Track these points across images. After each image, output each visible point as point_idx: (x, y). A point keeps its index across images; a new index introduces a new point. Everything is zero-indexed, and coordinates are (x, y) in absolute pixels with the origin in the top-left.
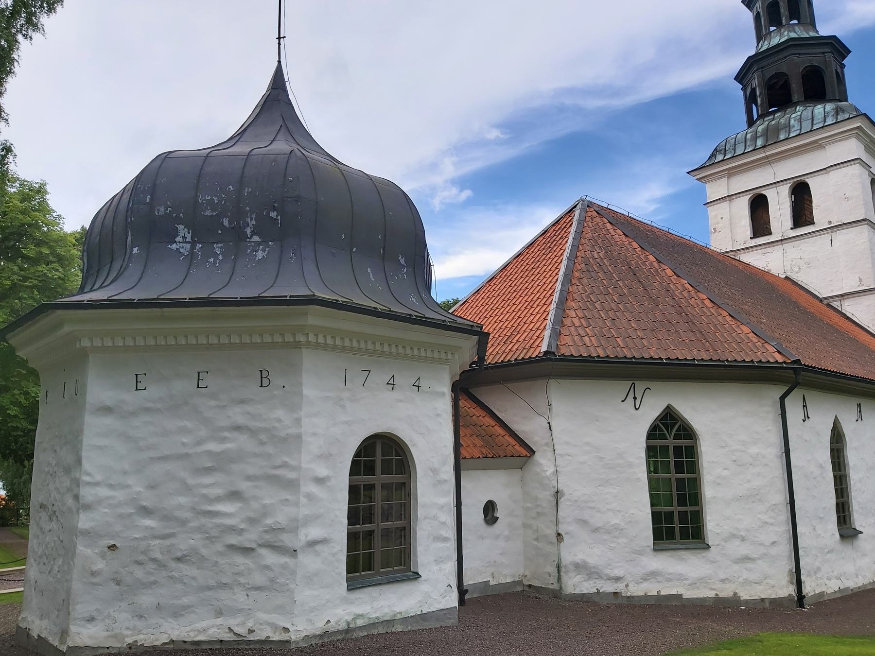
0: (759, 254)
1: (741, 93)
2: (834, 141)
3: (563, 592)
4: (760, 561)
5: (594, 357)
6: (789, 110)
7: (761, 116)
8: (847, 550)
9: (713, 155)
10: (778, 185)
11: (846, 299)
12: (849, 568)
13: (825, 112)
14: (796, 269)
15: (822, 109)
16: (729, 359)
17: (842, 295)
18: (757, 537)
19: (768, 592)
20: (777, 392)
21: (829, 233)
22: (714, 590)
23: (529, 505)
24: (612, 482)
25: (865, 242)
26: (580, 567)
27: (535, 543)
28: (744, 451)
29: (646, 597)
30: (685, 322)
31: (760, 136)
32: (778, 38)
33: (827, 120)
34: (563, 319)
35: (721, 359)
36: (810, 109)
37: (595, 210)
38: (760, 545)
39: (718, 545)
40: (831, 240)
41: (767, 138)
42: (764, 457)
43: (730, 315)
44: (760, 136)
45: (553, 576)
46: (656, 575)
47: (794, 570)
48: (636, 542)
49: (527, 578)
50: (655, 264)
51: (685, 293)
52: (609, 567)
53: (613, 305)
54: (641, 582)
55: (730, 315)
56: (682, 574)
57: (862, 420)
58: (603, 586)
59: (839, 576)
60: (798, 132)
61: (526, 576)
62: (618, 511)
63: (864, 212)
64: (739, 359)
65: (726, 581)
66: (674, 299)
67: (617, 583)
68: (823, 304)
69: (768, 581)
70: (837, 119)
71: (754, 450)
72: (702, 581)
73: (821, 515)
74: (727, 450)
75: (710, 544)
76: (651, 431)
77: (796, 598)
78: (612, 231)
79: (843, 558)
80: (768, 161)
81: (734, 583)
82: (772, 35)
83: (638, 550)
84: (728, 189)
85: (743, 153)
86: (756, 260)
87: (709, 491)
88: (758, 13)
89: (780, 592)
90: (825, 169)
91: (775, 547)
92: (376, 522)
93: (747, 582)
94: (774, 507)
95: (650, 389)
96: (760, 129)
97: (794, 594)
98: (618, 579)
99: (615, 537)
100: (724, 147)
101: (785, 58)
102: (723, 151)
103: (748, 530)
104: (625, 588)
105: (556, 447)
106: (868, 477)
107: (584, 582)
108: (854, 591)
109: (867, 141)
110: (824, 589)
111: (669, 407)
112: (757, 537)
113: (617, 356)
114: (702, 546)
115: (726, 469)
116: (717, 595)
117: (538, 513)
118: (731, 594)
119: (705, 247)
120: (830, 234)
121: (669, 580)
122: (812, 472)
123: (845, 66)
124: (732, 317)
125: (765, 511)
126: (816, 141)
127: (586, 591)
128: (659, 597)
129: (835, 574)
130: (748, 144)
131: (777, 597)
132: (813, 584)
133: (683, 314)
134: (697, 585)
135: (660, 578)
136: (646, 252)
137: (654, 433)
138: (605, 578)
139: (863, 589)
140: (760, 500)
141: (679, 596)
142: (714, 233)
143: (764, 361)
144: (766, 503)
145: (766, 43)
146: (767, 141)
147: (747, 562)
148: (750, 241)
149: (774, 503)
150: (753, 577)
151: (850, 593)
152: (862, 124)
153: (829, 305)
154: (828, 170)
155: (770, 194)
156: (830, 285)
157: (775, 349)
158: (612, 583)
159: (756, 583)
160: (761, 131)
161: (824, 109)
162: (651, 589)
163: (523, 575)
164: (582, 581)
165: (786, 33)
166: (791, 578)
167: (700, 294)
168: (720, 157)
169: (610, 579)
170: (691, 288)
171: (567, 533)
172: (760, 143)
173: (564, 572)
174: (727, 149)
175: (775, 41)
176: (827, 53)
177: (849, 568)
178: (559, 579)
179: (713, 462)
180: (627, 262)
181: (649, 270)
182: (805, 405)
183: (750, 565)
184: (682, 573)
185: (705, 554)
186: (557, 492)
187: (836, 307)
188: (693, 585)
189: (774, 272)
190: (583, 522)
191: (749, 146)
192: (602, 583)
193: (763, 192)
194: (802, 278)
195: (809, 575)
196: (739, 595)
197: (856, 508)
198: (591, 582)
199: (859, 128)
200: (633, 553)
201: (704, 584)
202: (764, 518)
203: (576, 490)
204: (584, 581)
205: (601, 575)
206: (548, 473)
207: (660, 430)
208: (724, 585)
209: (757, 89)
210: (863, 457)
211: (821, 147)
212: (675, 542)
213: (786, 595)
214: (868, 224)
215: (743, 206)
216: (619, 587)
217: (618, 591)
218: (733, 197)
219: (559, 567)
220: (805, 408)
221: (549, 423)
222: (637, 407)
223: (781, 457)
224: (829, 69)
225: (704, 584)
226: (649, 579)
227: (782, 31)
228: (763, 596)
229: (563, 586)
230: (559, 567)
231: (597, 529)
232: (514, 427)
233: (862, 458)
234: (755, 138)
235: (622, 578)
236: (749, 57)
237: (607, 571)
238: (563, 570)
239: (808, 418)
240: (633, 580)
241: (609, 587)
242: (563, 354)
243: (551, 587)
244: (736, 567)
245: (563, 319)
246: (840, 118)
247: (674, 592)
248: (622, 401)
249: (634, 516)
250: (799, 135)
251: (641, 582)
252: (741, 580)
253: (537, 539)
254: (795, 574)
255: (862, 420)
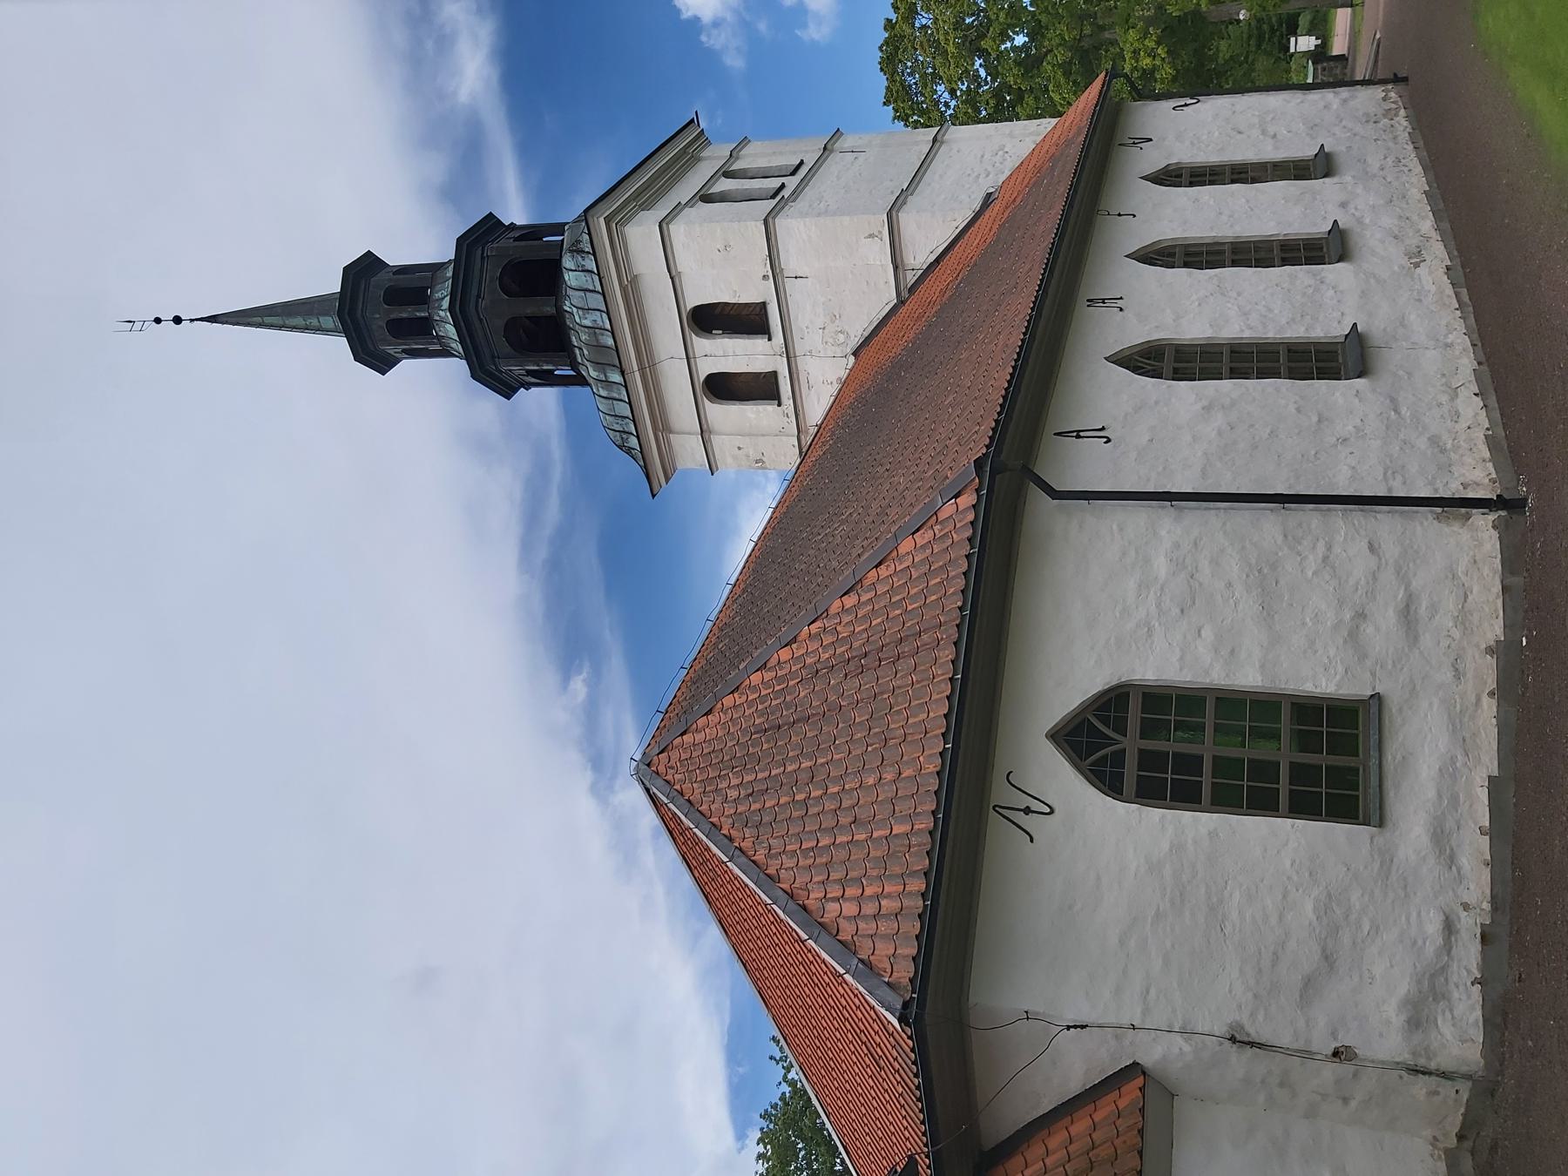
0: (809, 394)
1: (534, 390)
2: (702, 148)
3: (1480, 1073)
4: (1414, 583)
5: (925, 906)
6: (568, 323)
7: (574, 365)
8: (1391, 360)
9: (629, 451)
10: (691, 355)
11: (902, 261)
12: (1431, 360)
13: (576, 271)
14: (842, 338)
15: (570, 273)
16: (959, 604)
17: (896, 268)
18: (1358, 583)
19: (1488, 575)
20: (1039, 502)
21: (783, 282)
22: (1478, 699)
23: (1261, 1098)
24: (1215, 900)
25: (805, 224)
26: (1417, 1018)
27: (1353, 1104)
28: (1162, 589)
29: (1494, 864)
30: (877, 663)
31: (606, 376)
32: (448, 326)
33: (590, 269)
34: (838, 937)
35: (958, 622)
36: (570, 292)
37: (658, 754)
38: (1375, 579)
39: (1373, 674)
40: (796, 277)
41: (609, 365)
42: (1177, 546)
43: (876, 567)
44: (606, 376)
45: (1438, 1086)
46: (1442, 832)
47: (1439, 510)
48: (1361, 868)
49: (1440, 1138)
50: (768, 675)
51: (828, 640)
52: (1420, 942)
53: (830, 805)
54: (1459, 872)
55: (876, 567)
56: (1440, 770)
57: (1121, 298)
58: (1465, 968)
59: (1450, 391)
60: (604, 315)
61: (1434, 1137)
62: (1284, 897)
63: (753, 223)
64: (961, 582)
65: (1461, 667)
66: (833, 666)
67: (1458, 932)
68: (908, 298)
69: (1460, 570)
70: (589, 253)
71: (1161, 566)
72: (1457, 723)
73: (1315, 419)
74: (1157, 624)
75: (1370, 693)
76: (1109, 728)
77: (1503, 513)
78: (699, 737)
79: (1410, 374)
80: (649, 367)
81: (1464, 648)
82: (441, 334)
83: (1381, 865)
84: (689, 434)
85: (630, 403)
86: (817, 408)
87: (1249, 677)
88: (404, 351)
89: (1488, 547)
90: (672, 278)
91: (1383, 546)
92: (1320, 763)
93: (1463, 619)
94: (1290, 538)
95: (1011, 772)
96: (593, 374)
97: (1492, 517)
98: (1449, 927)
99: (1348, 916)
100: (618, 433)
101: (481, 320)
102: (624, 436)
103: (1341, 603)
104: (1472, 913)
105: (1126, 1021)
106: (1239, 294)
107: (1455, 1013)
108: (1483, 359)
109: (634, 207)
110: (1479, 435)
111: (1055, 736)
112: (1358, 583)
113: (927, 853)
114: (1374, 709)
115: (1199, 631)
116: (1491, 694)
117: (1281, 1085)
118: (1491, 661)
119: (774, 513)
120: (786, 279)
121: (1454, 801)
122: (1220, 433)
123: (512, 223)
124: (880, 564)
125: (1299, 559)
126: (623, 289)
127: (1478, 1013)
128: (1495, 832)
129: (1444, 399)
130: (616, 395)
131: (1499, 556)
132: (1468, 460)
133: (862, 661)
134: (1467, 736)
135: (1450, 824)
136: (743, 686)
137: (1108, 780)
138: (1446, 958)
139: (1475, 336)
140: (1274, 567)
141: (1494, 784)
142: (763, 462)
143: (971, 531)
144: (1280, 554)
145: (454, 345)
146: (614, 366)
147: (1415, 611)
148: (784, 407)
149: (1280, 539)
150: (1450, 604)
151: (1486, 368)
152: (601, 216)
153: (912, 290)
154: (674, 273)
155: (706, 368)
156: (875, 284)
157: (950, 502)
158: (1460, 943)
159: (1465, 601)
160: (596, 374)
161: (572, 270)
162: (1474, 849)
163: (1432, 1145)
164: (1453, 1018)
165: (442, 313)
166: (1455, 519)
167: (832, 611)
168: (633, 442)
169: (1448, 947)
170: (818, 624)
171: (1334, 1035)
172: (616, 377)
173: (1429, 1059)
174: (622, 429)
175: (451, 331)
176: (483, 253)
177: (1431, 360)
178: (1444, 1075)
179: (1182, 658)
180: (755, 733)
181: (777, 694)
182: (1075, 434)
183: (1423, 609)
184: (1438, 767)
185: (1394, 702)
186: (1233, 1039)
187: (915, 278)
188: (1466, 745)
189: (843, 374)
190: (1309, 988)
191: (620, 394)
192: (1459, 967)
193: (702, 379)
194: (859, 328)
195: (1447, 468)
196: (1492, 643)
197: (1303, 329)
198: (1456, 995)
199: (608, 221)
200: (1387, 879)
201: (1466, 720)
202: (1312, 563)
203: (1230, 991)
204: (1451, 1011)
205: (1438, 966)
206: (1187, 1048)
207: (1102, 761)
208: (1470, 675)
209: (527, 368)
210: (1197, 303)
211: (635, 280)
212: (1364, 770)
213: (1495, 534)
214: (774, 218)
215: (723, 414)
216: (1469, 926)
217: (1479, 931)
218: (705, 427)
219: (1415, 1071)
220: (1082, 434)
221: (1069, 1028)
222: (1049, 810)
223: (1181, 509)
224: (511, 253)
225: (1466, 720)
226: (1452, 849)
227: (438, 318)
228: (1497, 588)
229: (1464, 1069)
230: (1415, 1071)
231: (1326, 958)
232: (1075, 1086)
233: (1199, 305)
234: (608, 383)
235: (1447, 918)
236: (472, 376)
237: (1430, 950)
238: (1422, 1062)
239: (1103, 429)
240: (1453, 890)
241: (1469, 954)
242: (911, 980)
243: (1465, 1096)
244: (1426, 640)
245: (838, 937)
246: (588, 248)
247: (1483, 795)
248: (1032, 841)
249: (1298, 862)
250: (608, 314)
251: (1459, 872)
252: (1456, 634)
253: (1345, 1100)
254: (1445, 509)
255: (1121, 298)
